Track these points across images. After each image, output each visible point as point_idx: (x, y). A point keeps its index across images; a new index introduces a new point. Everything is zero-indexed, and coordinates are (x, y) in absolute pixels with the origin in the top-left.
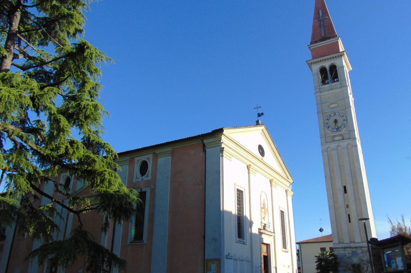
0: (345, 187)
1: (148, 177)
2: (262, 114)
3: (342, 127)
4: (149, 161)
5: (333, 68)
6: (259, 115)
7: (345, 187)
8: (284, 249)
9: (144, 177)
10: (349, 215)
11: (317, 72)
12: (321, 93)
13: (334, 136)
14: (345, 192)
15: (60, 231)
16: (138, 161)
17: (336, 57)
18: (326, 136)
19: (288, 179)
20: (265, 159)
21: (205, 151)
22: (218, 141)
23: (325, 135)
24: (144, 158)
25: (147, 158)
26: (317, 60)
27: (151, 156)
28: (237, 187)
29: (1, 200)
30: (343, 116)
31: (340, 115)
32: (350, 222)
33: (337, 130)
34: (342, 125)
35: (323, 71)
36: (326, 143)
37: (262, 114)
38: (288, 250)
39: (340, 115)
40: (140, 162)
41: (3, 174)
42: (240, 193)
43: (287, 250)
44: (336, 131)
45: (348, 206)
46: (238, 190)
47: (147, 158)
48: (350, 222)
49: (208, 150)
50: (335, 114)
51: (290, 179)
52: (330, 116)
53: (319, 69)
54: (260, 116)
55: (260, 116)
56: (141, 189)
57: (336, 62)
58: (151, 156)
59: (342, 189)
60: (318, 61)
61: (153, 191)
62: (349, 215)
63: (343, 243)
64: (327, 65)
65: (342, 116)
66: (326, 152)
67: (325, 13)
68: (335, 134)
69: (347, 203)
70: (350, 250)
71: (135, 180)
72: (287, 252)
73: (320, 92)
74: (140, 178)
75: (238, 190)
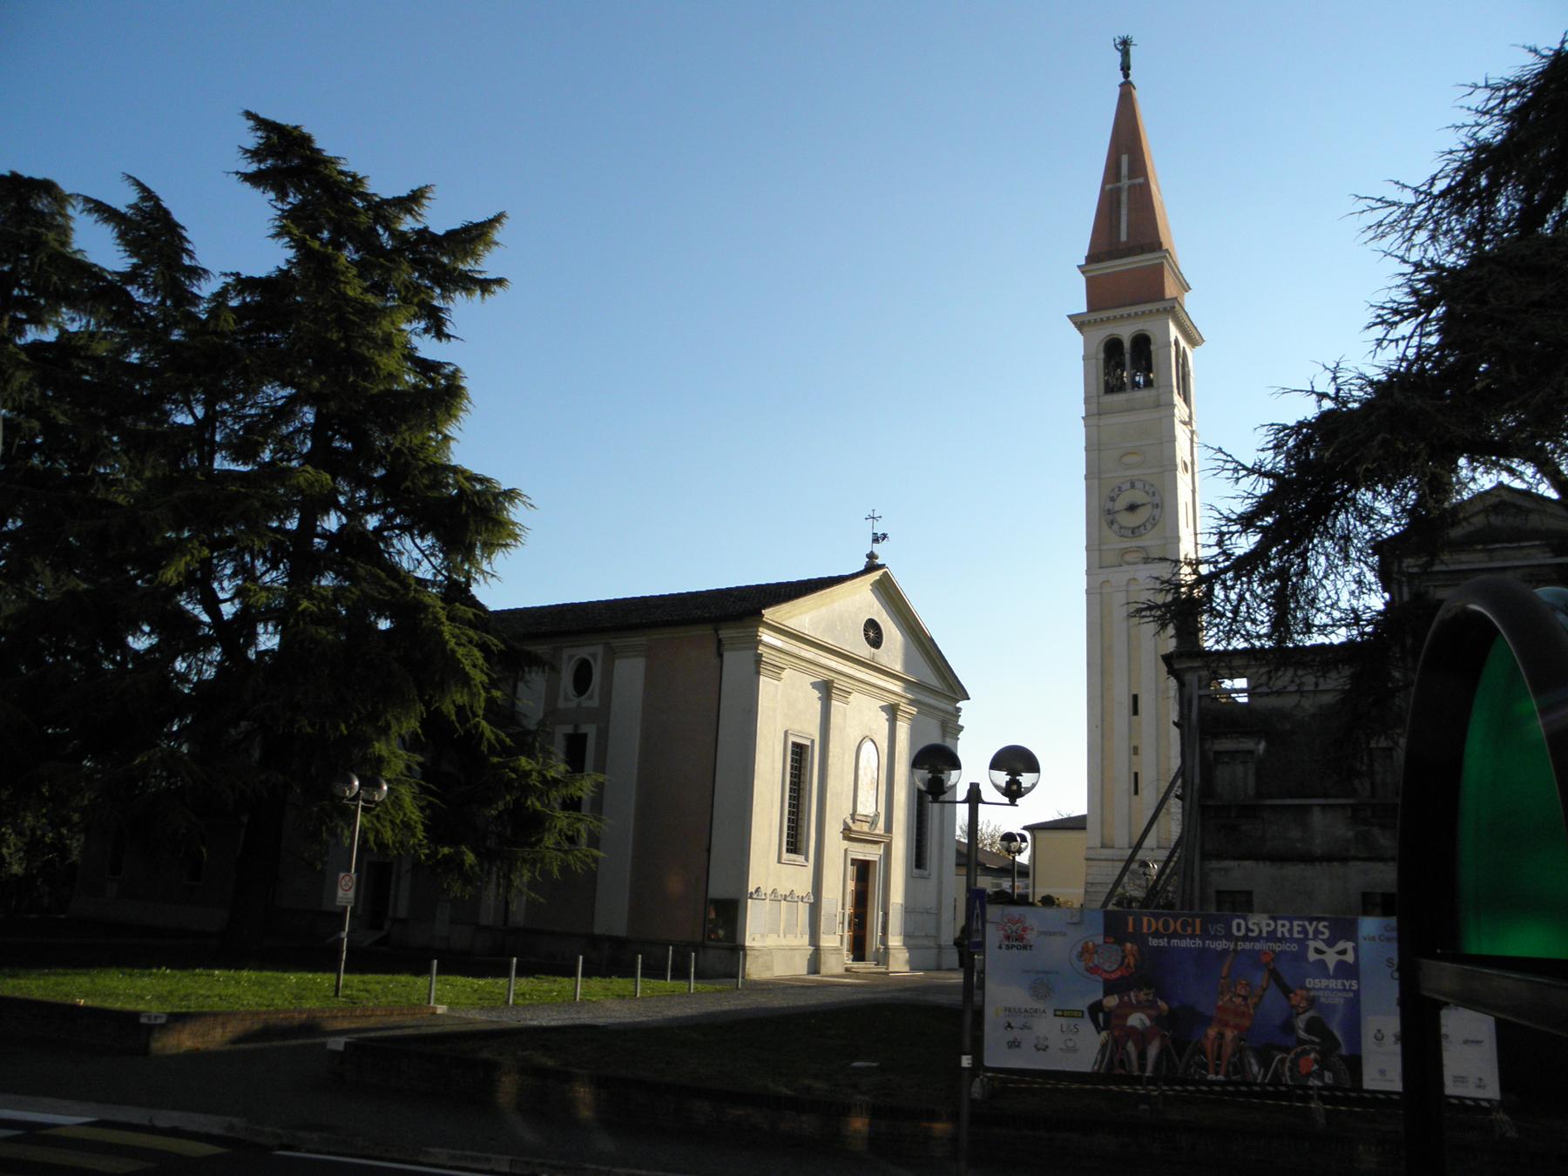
0: (1135, 698)
1: (592, 701)
2: (884, 536)
3: (1149, 526)
4: (595, 660)
5: (1142, 343)
7: (1135, 698)
8: (915, 871)
9: (583, 697)
10: (1136, 775)
11: (1097, 354)
13: (1125, 552)
14: (1135, 711)
16: (571, 657)
17: (1151, 312)
18: (1104, 547)
21: (721, 656)
23: (1100, 545)
24: (583, 652)
25: (589, 654)
26: (1104, 314)
27: (599, 650)
28: (791, 739)
30: (1154, 493)
31: (1147, 489)
32: (1136, 792)
33: (1133, 533)
34: (1148, 520)
35: (1113, 348)
36: (1101, 568)
37: (884, 536)
39: (1147, 489)
40: (573, 662)
42: (799, 754)
43: (926, 873)
44: (1130, 535)
45: (1136, 751)
47: (589, 654)
48: (1136, 792)
49: (727, 656)
50: (1133, 486)
52: (1120, 489)
53: (1103, 344)
56: (576, 727)
57: (1148, 326)
58: (599, 650)
59: (1127, 704)
60: (1102, 320)
61: (603, 735)
62: (1136, 775)
63: (1113, 847)
64: (1126, 332)
65: (1151, 492)
66: (1098, 596)
67: (1139, 166)
68: (1128, 545)
69: (1135, 743)
70: (948, 903)
71: (561, 704)
74: (574, 702)
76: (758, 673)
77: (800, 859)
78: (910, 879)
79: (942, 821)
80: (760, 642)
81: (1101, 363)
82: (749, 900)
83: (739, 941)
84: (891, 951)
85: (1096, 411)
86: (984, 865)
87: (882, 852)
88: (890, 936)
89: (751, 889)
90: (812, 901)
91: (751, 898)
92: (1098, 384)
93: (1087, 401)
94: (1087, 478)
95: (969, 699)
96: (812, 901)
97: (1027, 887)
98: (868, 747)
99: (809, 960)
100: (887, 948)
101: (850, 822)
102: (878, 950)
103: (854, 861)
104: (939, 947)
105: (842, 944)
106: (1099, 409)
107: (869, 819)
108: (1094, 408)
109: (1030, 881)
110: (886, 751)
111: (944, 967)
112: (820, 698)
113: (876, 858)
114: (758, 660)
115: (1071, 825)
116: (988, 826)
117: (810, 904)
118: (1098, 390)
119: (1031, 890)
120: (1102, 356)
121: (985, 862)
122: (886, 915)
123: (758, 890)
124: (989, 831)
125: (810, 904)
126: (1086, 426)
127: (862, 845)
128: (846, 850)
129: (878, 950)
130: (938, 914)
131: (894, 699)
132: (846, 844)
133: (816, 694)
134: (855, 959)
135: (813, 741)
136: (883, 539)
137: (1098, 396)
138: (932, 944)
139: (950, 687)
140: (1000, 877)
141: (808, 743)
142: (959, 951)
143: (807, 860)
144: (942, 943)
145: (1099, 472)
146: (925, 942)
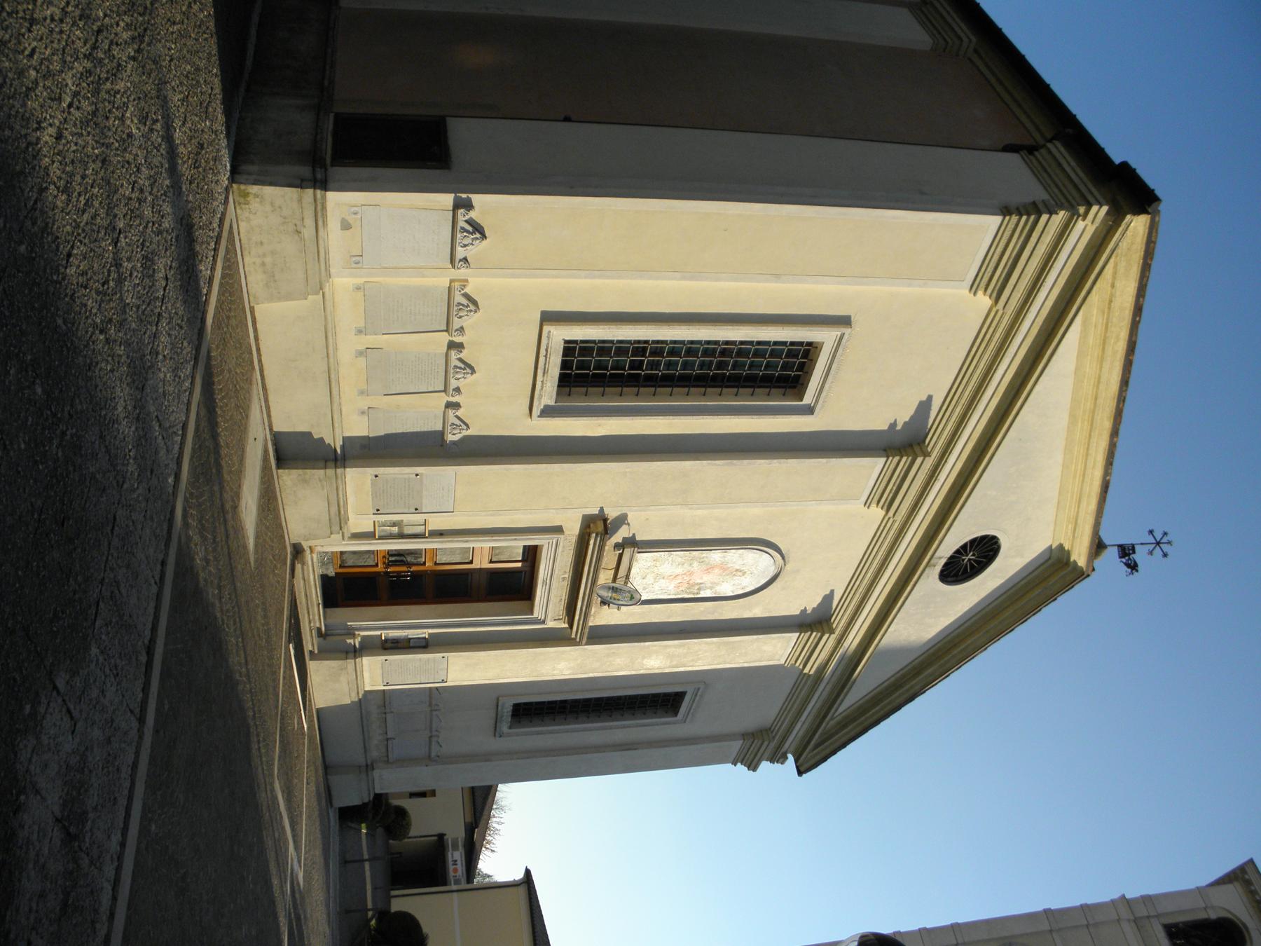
2: (1133, 567)
6: (1126, 551)
8: (507, 709)
12: (1133, 924)
15: (628, 524)
19: (817, 746)
20: (929, 582)
22: (1074, 192)
29: (873, 938)
37: (1133, 567)
38: (509, 735)
41: (1115, 439)
43: (505, 728)
46: (804, 355)
51: (816, 754)
53: (1229, 916)
54: (1120, 557)
55: (1120, 557)
72: (496, 731)
73: (1135, 921)
75: (804, 355)
76: (1005, 211)
77: (548, 393)
78: (493, 693)
79: (598, 749)
80: (1074, 216)
81: (1202, 916)
82: (447, 199)
83: (337, 172)
84: (350, 662)
85: (1139, 915)
86: (477, 827)
87: (551, 624)
88: (380, 659)
89: (486, 205)
90: (450, 438)
91: (458, 205)
92: (1172, 913)
93: (1147, 900)
94: (1047, 912)
95: (800, 773)
96: (450, 438)
97: (457, 882)
98: (758, 565)
99: (308, 435)
100: (356, 652)
101: (618, 538)
102: (351, 633)
103: (531, 554)
104: (369, 767)
105: (357, 536)
106: (1141, 918)
107: (619, 583)
108: (1142, 912)
109: (464, 886)
110: (747, 614)
111: (334, 780)
112: (893, 425)
113: (538, 612)
114: (1035, 209)
115: (538, 929)
116: (498, 823)
117: (441, 434)
118: (1167, 914)
119: (454, 887)
120: (1213, 916)
121: (479, 829)
122: (423, 646)
123: (478, 229)
124: (494, 825)
125: (441, 434)
126: (1113, 901)
127: (568, 576)
128: (558, 530)
129: (351, 633)
130: (429, 759)
131: (839, 623)
132: (573, 528)
133: (903, 415)
134: (326, 581)
135: (810, 410)
136: (1128, 565)
137: (1157, 916)
138: (374, 754)
139: (829, 736)
140: (465, 846)
141: (808, 399)
142: (365, 805)
143: (547, 412)
144: (376, 773)
145: (1059, 930)
146: (376, 738)
